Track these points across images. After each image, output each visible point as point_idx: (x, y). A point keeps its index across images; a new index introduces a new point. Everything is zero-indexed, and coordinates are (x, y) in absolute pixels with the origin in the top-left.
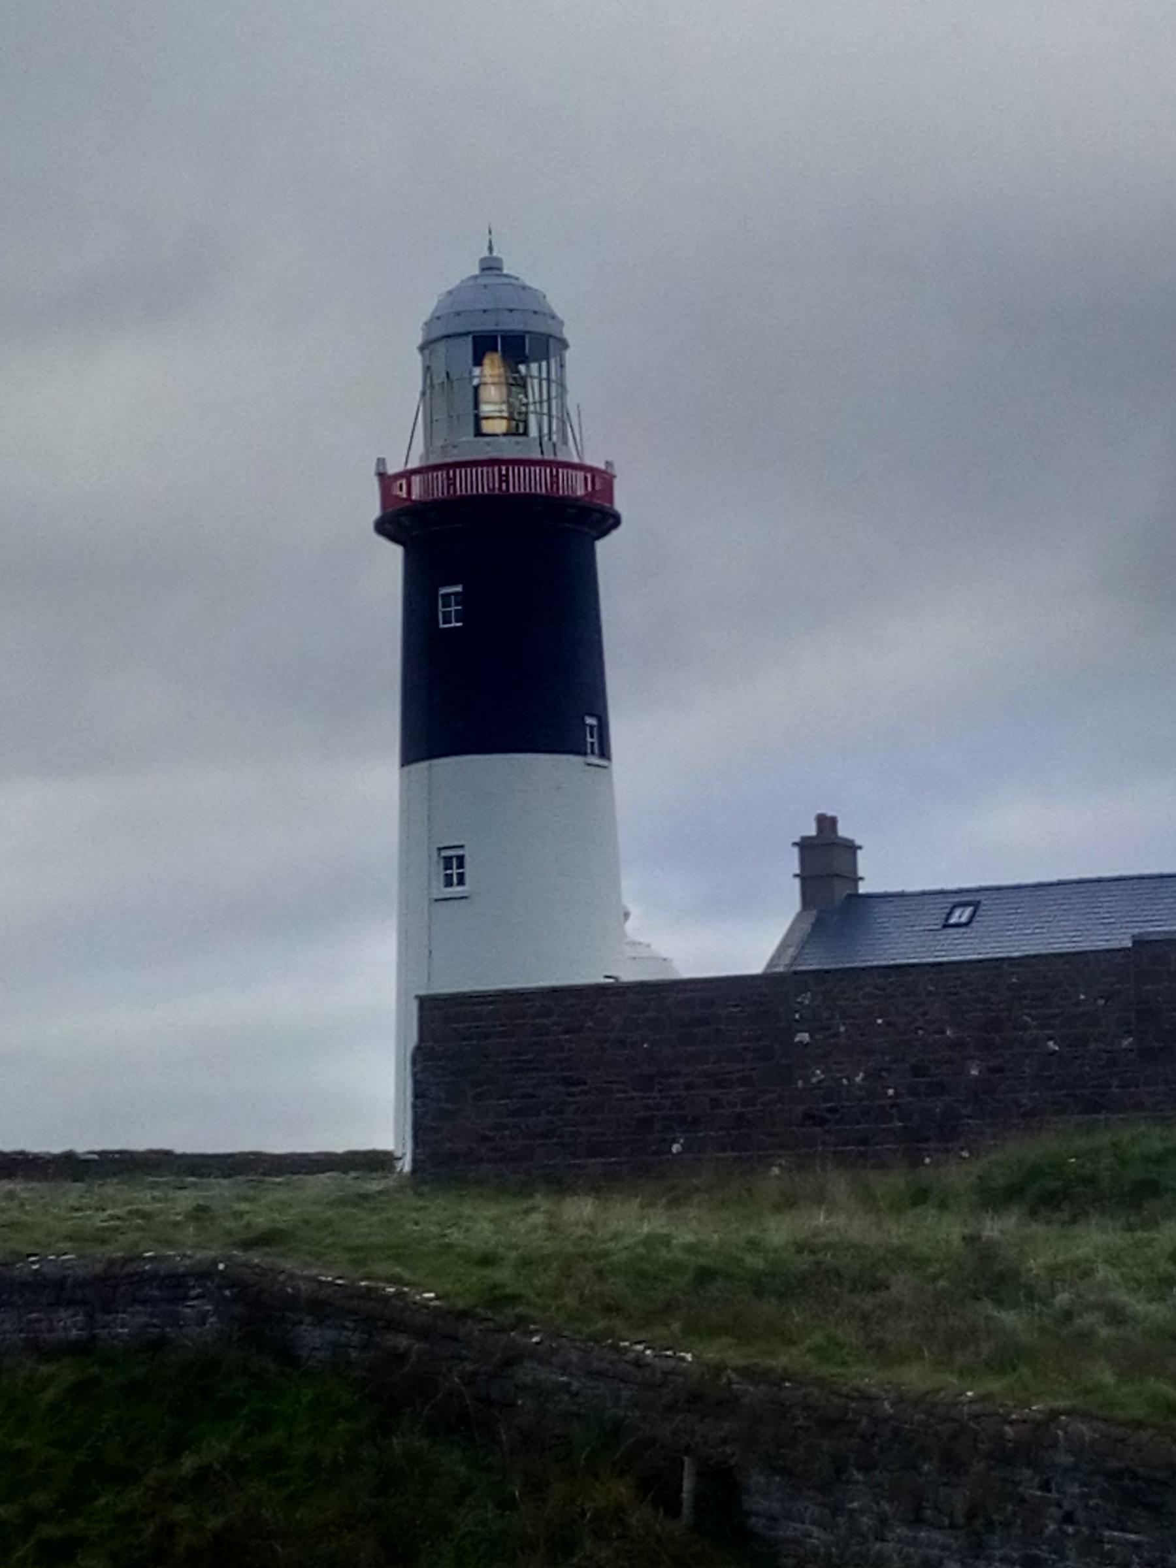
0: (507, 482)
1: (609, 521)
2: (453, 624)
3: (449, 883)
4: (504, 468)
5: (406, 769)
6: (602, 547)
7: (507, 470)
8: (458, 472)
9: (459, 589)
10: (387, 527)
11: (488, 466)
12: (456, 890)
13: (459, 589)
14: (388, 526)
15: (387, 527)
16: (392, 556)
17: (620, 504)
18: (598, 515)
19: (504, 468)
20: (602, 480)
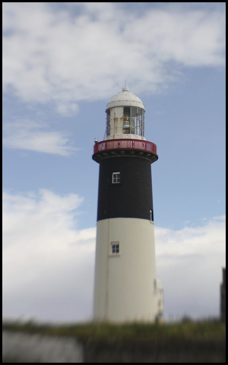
0: (134, 145)
1: (154, 158)
2: (117, 183)
3: (114, 251)
4: (133, 141)
5: (100, 221)
6: (153, 165)
7: (134, 142)
8: (135, 142)
9: (119, 173)
10: (95, 157)
11: (106, 142)
12: (115, 254)
13: (119, 173)
14: (95, 158)
15: (95, 157)
16: (96, 166)
17: (158, 153)
18: (154, 157)
19: (119, 142)
20: (154, 147)
